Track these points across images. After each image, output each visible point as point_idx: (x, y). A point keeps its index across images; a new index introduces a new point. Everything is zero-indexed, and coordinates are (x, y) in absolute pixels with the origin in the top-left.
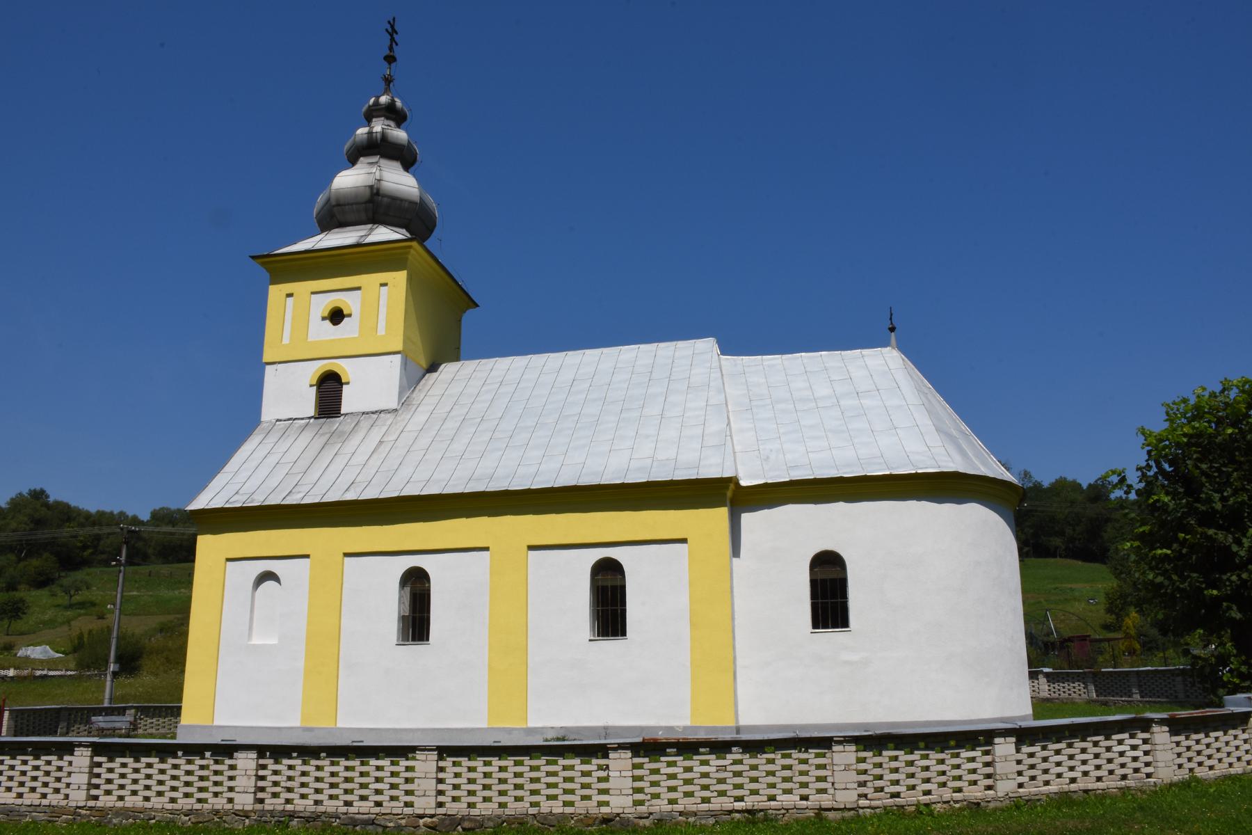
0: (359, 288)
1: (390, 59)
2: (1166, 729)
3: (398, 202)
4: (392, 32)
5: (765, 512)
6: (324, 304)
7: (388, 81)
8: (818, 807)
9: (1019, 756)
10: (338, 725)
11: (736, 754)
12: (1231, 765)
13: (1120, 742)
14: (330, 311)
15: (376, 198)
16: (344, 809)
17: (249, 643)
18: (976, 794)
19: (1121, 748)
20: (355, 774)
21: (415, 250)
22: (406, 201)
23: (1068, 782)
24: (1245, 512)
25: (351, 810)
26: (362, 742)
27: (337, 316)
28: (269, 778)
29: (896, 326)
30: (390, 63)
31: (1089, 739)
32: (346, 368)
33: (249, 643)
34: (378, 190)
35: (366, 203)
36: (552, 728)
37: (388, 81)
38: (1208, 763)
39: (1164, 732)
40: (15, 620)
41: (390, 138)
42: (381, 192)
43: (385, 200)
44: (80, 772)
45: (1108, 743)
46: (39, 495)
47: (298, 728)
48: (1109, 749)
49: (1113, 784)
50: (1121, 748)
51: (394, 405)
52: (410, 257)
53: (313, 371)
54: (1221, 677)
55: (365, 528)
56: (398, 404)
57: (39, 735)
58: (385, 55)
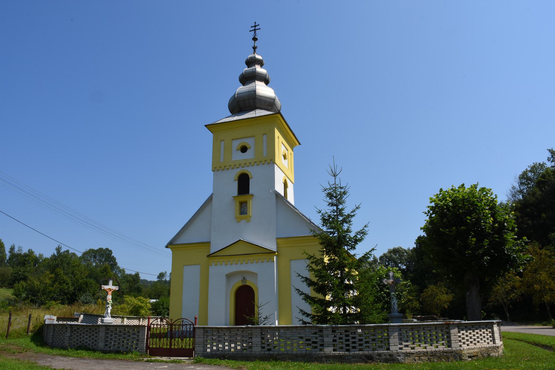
1: (255, 39)
6: (237, 144)
7: (255, 48)
8: (232, 353)
9: (459, 334)
14: (241, 147)
16: (267, 352)
18: (419, 350)
20: (351, 340)
25: (271, 352)
26: (112, 323)
27: (244, 149)
28: (351, 340)
30: (255, 41)
32: (250, 171)
37: (255, 48)
40: (140, 277)
53: (235, 174)
54: (332, 300)
57: (484, 320)
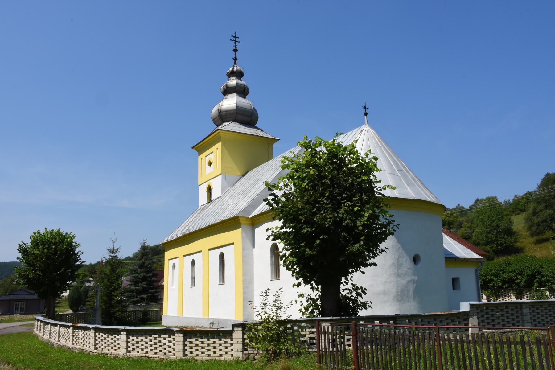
0: (213, 152)
1: (235, 50)
2: (182, 335)
3: (229, 112)
4: (235, 39)
5: (208, 238)
7: (235, 60)
10: (184, 316)
11: (60, 332)
12: (103, 349)
13: (165, 339)
15: (220, 113)
17: (172, 288)
19: (165, 341)
21: (221, 132)
22: (231, 110)
23: (145, 353)
24: (49, 261)
29: (368, 113)
31: (152, 336)
33: (172, 288)
34: (220, 110)
35: (218, 117)
36: (212, 318)
37: (235, 60)
38: (164, 351)
39: (180, 336)
41: (229, 86)
42: (222, 111)
43: (224, 113)
44: (528, 322)
45: (160, 339)
46: (548, 175)
47: (176, 316)
48: (160, 341)
49: (134, 354)
50: (165, 341)
51: (220, 195)
52: (221, 136)
55: (186, 246)
56: (222, 194)
58: (233, 49)
